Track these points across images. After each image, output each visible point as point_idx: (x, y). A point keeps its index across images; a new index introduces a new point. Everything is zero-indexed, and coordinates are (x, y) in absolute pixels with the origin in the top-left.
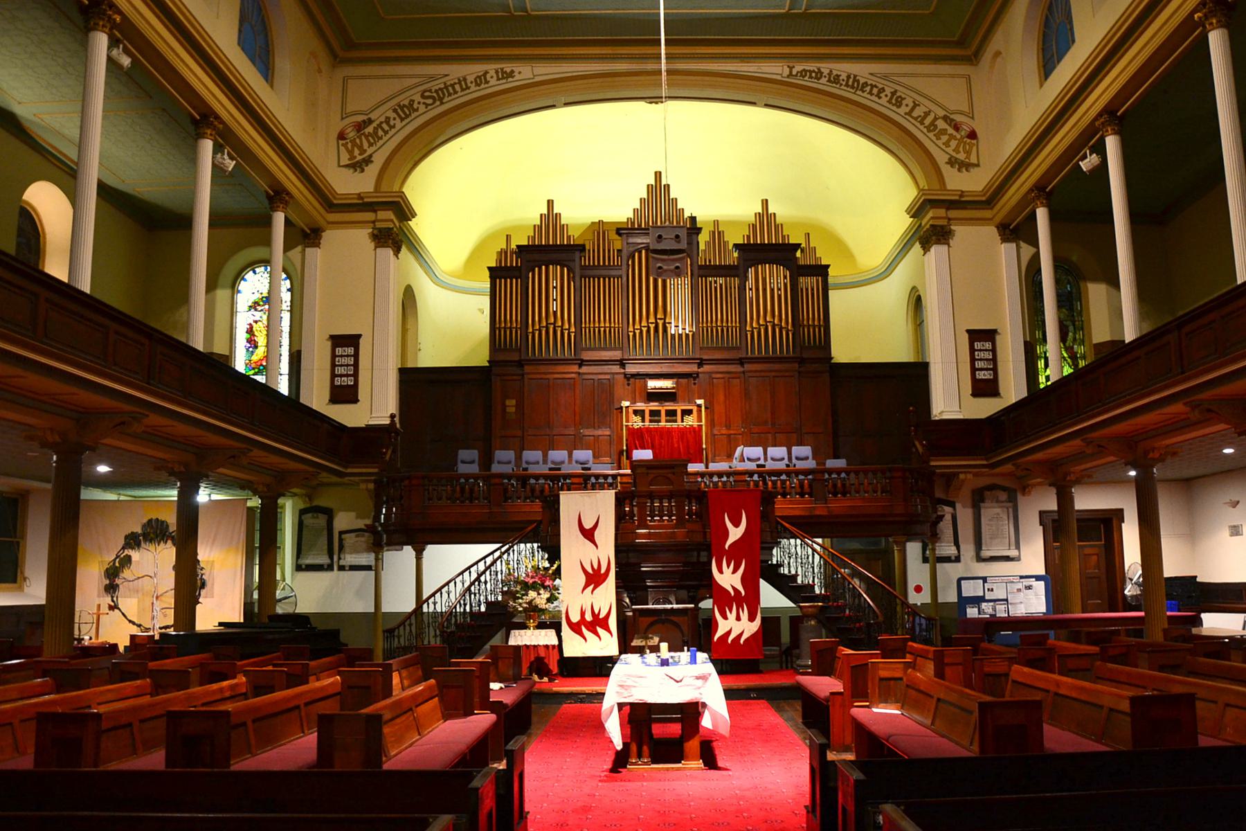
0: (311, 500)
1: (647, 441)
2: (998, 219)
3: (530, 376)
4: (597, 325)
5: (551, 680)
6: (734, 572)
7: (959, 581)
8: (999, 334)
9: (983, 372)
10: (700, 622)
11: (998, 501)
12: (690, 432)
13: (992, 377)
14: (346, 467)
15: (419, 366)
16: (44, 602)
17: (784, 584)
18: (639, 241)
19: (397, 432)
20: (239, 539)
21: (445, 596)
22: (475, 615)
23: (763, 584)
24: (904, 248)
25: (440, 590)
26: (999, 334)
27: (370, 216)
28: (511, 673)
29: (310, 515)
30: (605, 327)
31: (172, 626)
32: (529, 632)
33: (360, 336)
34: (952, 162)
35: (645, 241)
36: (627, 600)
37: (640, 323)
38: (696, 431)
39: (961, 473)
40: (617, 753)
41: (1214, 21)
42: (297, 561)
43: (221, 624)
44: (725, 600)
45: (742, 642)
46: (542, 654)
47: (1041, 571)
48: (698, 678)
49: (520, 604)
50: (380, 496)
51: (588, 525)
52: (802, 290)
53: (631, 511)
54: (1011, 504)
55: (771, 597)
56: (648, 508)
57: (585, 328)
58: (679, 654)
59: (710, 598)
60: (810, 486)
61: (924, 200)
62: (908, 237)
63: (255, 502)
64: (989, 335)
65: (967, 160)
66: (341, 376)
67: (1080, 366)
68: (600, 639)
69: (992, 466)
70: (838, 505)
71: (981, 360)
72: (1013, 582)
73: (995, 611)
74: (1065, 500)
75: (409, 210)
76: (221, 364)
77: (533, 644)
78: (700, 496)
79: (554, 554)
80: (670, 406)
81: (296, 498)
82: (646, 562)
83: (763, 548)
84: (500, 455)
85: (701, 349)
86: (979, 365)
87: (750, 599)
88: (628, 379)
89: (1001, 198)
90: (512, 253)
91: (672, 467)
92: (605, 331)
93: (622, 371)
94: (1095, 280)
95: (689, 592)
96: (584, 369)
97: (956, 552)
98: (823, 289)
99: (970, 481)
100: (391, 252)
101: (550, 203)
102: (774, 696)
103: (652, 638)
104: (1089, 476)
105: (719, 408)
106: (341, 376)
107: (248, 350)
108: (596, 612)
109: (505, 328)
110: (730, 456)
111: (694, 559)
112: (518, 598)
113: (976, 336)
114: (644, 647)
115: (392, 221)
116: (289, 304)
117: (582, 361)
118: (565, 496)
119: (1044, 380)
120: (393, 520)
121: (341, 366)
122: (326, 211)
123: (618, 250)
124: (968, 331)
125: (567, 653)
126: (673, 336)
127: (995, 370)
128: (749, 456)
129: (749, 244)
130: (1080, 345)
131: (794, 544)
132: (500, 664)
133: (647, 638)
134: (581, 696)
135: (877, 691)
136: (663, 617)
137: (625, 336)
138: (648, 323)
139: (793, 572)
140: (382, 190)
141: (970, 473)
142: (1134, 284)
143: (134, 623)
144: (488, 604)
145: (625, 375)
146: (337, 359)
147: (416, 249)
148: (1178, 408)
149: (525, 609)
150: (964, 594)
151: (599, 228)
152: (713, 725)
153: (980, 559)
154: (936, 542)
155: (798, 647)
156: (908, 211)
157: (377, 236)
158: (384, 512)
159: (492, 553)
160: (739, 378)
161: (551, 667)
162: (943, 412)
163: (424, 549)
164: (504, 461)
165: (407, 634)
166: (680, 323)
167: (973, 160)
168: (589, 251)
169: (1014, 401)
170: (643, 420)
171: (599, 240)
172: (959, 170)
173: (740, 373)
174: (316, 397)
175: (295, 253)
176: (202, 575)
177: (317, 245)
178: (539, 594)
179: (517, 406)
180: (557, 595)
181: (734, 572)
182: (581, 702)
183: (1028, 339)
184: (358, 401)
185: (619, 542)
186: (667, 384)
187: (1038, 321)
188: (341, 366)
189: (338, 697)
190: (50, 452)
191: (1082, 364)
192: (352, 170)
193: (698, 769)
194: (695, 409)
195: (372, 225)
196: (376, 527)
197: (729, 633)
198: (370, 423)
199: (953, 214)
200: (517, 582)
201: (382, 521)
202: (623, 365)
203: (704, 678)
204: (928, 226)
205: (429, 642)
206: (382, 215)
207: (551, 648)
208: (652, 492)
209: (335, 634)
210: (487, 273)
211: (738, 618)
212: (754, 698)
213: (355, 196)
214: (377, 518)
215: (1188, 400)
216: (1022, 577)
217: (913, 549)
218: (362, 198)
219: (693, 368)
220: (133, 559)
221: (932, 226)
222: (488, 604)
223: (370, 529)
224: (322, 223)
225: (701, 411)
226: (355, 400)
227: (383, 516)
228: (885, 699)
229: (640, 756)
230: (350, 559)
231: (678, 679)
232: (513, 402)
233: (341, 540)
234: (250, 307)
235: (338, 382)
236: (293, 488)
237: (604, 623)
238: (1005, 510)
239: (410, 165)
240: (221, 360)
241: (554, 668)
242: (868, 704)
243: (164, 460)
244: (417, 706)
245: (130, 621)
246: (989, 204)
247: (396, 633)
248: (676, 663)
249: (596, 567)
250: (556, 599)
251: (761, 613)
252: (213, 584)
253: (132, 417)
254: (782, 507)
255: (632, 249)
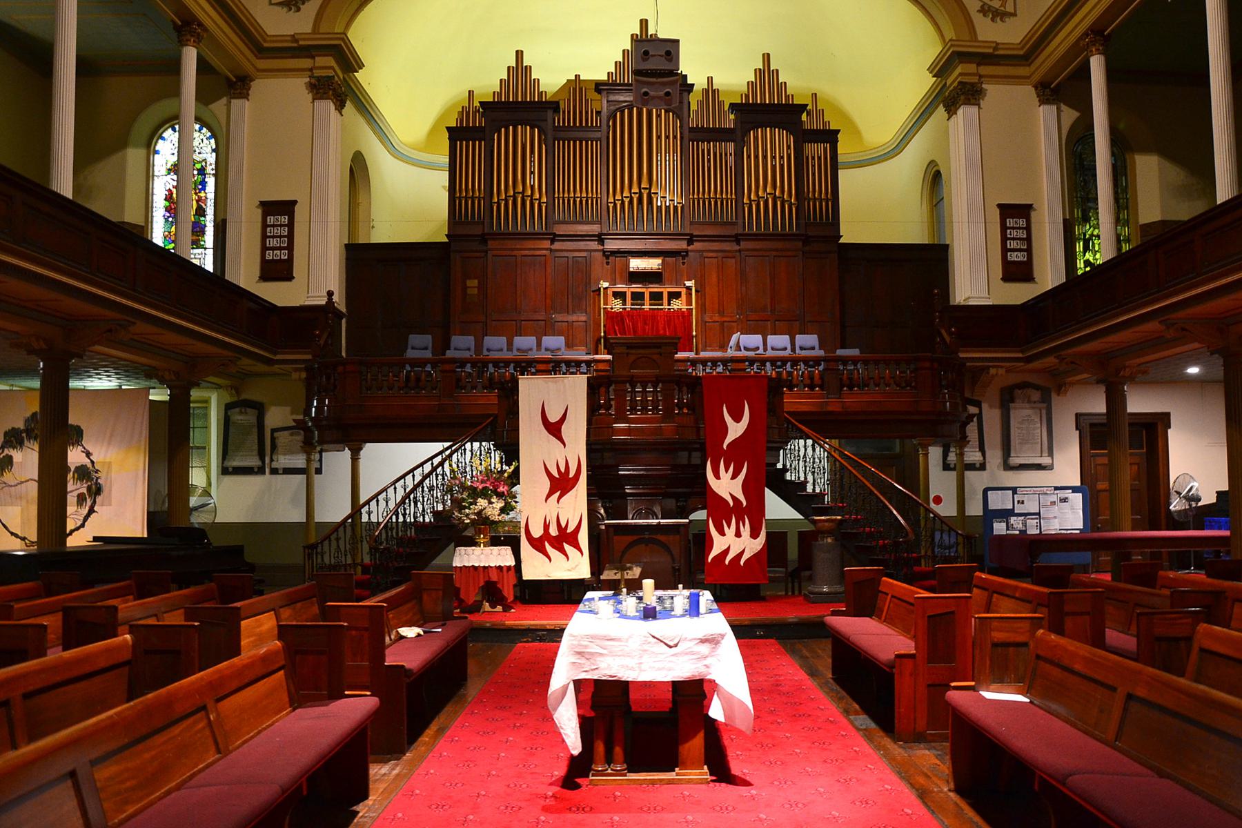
0: (238, 391)
1: (629, 327)
2: (1036, 77)
3: (495, 253)
4: (572, 195)
5: (507, 608)
6: (734, 477)
7: (986, 491)
8: (1035, 210)
9: (1016, 253)
10: (691, 537)
11: (1029, 402)
12: (678, 317)
13: (1025, 259)
14: (275, 354)
15: (372, 242)
16: (1227, 489)
17: (792, 493)
18: (622, 98)
19: (339, 315)
20: (141, 433)
21: (382, 504)
22: (420, 527)
23: (770, 496)
24: (923, 114)
25: (376, 496)
26: (1035, 210)
27: (306, 63)
28: (440, 609)
29: (237, 410)
30: (581, 197)
31: (36, 542)
32: (477, 550)
33: (294, 203)
34: (985, 10)
35: (628, 99)
36: (602, 511)
37: (622, 193)
38: (685, 316)
39: (993, 367)
40: (572, 758)
41: (1094, 50)
42: (223, 463)
43: (96, 539)
44: (722, 512)
45: (742, 563)
46: (494, 578)
47: (1077, 482)
48: (703, 641)
49: (467, 515)
50: (312, 389)
51: (553, 418)
52: (807, 158)
53: (608, 400)
54: (1045, 405)
55: (777, 508)
56: (628, 403)
57: (559, 198)
58: (670, 592)
59: (702, 508)
60: (821, 378)
61: (953, 52)
62: (914, 121)
63: (159, 395)
64: (1023, 211)
65: (1002, 8)
66: (273, 249)
67: (1124, 251)
68: (568, 558)
69: (1028, 360)
70: (853, 400)
71: (1013, 239)
72: (1046, 494)
73: (1026, 526)
74: (1116, 400)
75: (354, 57)
76: (138, 236)
77: (482, 565)
78: (694, 384)
79: (511, 452)
80: (655, 288)
81: (221, 390)
82: (625, 463)
83: (769, 449)
84: (457, 340)
85: (692, 223)
86: (1011, 244)
87: (753, 511)
88: (607, 257)
89: (1046, 47)
90: (476, 111)
91: (658, 346)
92: (581, 202)
93: (601, 247)
94: (1146, 149)
95: (677, 502)
96: (557, 246)
97: (982, 459)
98: (831, 158)
99: (1000, 376)
100: (332, 107)
101: (519, 55)
102: (787, 634)
103: (630, 569)
104: (1144, 372)
105: (711, 291)
106: (273, 249)
107: (166, 220)
108: (563, 525)
109: (466, 198)
110: (723, 346)
111: (685, 462)
112: (465, 508)
113: (1007, 211)
114: (619, 581)
115: (332, 68)
116: (213, 166)
117: (555, 235)
118: (525, 381)
119: (1082, 266)
120: (326, 414)
121: (273, 237)
122: (256, 56)
123: (597, 112)
124: (1000, 206)
125: (527, 575)
126: (659, 208)
127: (1029, 250)
128: (747, 342)
129: (747, 104)
130: (1124, 226)
131: (800, 445)
132: (425, 597)
133: (623, 569)
134: (540, 633)
135: (988, 662)
136: (647, 537)
137: (604, 207)
138: (630, 193)
139: (802, 479)
140: (321, 31)
141: (1002, 367)
142: (1232, 130)
143: (16, 536)
144: (436, 514)
145: (604, 252)
146: (268, 229)
147: (365, 108)
148: (1153, 326)
149: (473, 521)
150: (991, 507)
151: (576, 86)
152: (725, 716)
153: (1008, 467)
154: (965, 446)
155: (810, 568)
156: (930, 70)
157: (315, 85)
158: (315, 404)
159: (441, 453)
160: (734, 257)
161: (505, 594)
162: (969, 298)
163: (361, 449)
164: (462, 345)
165: (333, 551)
166: (668, 195)
167: (1010, 8)
168: (564, 112)
169: (1050, 288)
170: (624, 304)
171: (575, 100)
172: (993, 20)
173: (736, 251)
174: (244, 274)
175: (219, 107)
176: (97, 478)
177: (245, 95)
178: (491, 503)
179: (479, 288)
180: (513, 503)
181: (734, 477)
182: (541, 641)
183: (1068, 217)
184: (294, 278)
185: (592, 438)
186: (653, 264)
187: (1077, 197)
188: (273, 237)
189: (127, 668)
190: (40, 360)
191: (1126, 247)
192: (285, 9)
193: (701, 782)
194: (684, 291)
195: (309, 73)
196: (306, 423)
197: (727, 551)
198: (306, 303)
199: (984, 70)
200: (463, 487)
201: (313, 415)
202: (601, 241)
203: (713, 641)
204: (956, 84)
205: (362, 560)
206: (321, 61)
207: (505, 569)
208: (633, 376)
209: (237, 551)
210: (447, 135)
211: (738, 534)
212: (761, 637)
213: (289, 38)
214: (307, 412)
215: (1162, 319)
216: (1056, 488)
217: (935, 453)
218: (297, 41)
219: (683, 245)
220: (15, 460)
221: (960, 83)
222: (436, 514)
223: (300, 425)
224: (249, 68)
225: (691, 294)
226: (289, 278)
227: (314, 409)
228: (1000, 678)
229: (609, 760)
230: (283, 461)
231: (671, 644)
232: (475, 283)
233: (273, 439)
234: (169, 170)
235: (270, 255)
236: (208, 376)
237: (572, 539)
238: (1038, 411)
239: (355, 6)
240: (135, 231)
241: (509, 593)
242: (973, 683)
243: (155, 367)
244: (218, 700)
245: (12, 534)
246: (1027, 60)
247: (319, 550)
248: (668, 613)
249: (563, 470)
250: (513, 509)
251: (766, 528)
252: (111, 490)
253: (230, 360)
254: (793, 401)
255: (612, 108)
